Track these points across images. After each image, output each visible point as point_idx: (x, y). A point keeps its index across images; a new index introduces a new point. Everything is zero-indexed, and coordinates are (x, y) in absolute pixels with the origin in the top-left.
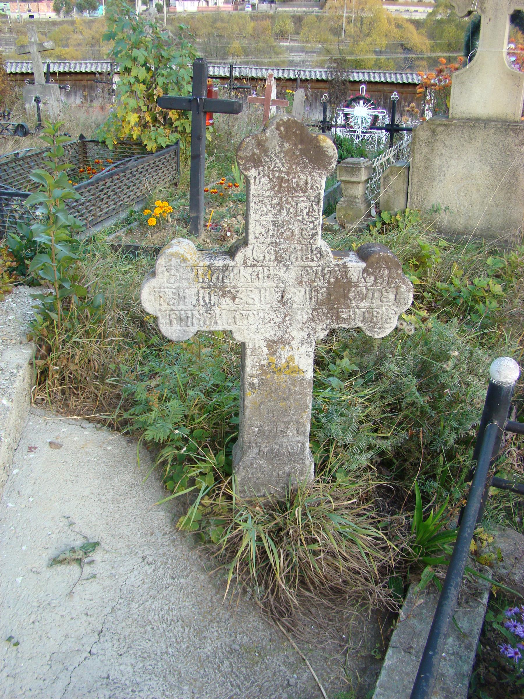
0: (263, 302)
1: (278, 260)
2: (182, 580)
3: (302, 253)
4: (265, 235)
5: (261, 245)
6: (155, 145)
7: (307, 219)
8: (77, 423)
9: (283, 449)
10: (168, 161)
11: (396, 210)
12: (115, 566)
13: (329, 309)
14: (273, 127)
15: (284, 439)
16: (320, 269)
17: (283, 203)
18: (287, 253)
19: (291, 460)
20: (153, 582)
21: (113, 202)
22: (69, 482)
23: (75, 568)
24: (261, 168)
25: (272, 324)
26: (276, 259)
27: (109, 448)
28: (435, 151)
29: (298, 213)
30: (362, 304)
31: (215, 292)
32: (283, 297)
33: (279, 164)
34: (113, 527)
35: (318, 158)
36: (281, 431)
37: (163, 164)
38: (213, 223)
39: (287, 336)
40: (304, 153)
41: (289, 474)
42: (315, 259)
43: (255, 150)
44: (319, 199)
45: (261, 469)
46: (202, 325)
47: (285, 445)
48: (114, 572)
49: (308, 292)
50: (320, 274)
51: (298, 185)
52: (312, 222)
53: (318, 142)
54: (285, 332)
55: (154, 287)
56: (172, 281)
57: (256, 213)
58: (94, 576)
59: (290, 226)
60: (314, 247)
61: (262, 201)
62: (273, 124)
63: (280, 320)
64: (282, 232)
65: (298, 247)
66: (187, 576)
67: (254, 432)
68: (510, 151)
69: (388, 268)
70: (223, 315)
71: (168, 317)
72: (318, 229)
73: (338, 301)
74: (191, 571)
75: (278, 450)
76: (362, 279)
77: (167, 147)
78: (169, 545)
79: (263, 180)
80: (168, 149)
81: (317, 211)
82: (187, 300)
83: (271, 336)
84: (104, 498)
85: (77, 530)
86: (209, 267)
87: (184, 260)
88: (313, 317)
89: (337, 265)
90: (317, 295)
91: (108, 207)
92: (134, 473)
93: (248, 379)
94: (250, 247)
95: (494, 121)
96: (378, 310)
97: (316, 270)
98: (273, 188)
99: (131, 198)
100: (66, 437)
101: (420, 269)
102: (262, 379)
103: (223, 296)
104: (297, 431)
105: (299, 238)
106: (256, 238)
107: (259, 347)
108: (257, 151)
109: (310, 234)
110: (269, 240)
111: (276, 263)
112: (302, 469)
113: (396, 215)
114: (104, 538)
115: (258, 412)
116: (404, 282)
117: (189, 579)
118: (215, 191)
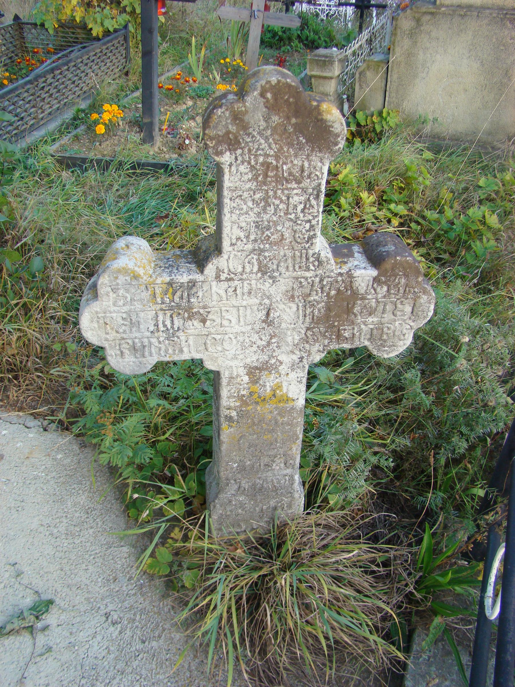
0: (242, 323)
1: (262, 271)
2: (154, 644)
3: (294, 260)
4: (245, 240)
5: (239, 254)
6: (101, 29)
7: (302, 218)
8: (20, 421)
9: (267, 483)
10: (117, 49)
11: (372, 109)
12: (74, 630)
13: (328, 327)
14: (255, 93)
15: (269, 474)
16: (318, 279)
17: (269, 197)
18: (274, 261)
19: (277, 494)
20: (120, 650)
21: (56, 101)
22: (13, 511)
23: (26, 638)
24: (239, 152)
25: (255, 348)
26: (259, 270)
27: (59, 456)
28: (418, 44)
29: (290, 210)
30: (370, 319)
31: (179, 314)
32: (268, 314)
33: (264, 145)
34: (69, 573)
35: (318, 135)
36: (265, 465)
37: (111, 52)
38: (169, 126)
39: (273, 361)
40: (299, 129)
41: (275, 509)
42: (312, 268)
43: (230, 127)
44: (319, 191)
45: (242, 505)
46: (163, 354)
47: (269, 479)
48: (72, 640)
49: (301, 308)
50: (317, 286)
51: (290, 174)
52: (309, 221)
53: (320, 114)
54: (271, 357)
55: (97, 313)
56: (121, 303)
57: (232, 212)
58: (49, 649)
59: (279, 228)
60: (311, 252)
61: (241, 196)
62: (255, 89)
63: (264, 343)
64: (267, 236)
65: (289, 254)
66: (160, 637)
67: (232, 468)
68: (504, 45)
69: (406, 276)
70: (191, 342)
71: (118, 348)
72: (317, 230)
73: (339, 316)
74: (164, 630)
75: (262, 485)
76: (372, 290)
77: (116, 31)
78: (135, 593)
79: (243, 168)
80: (116, 34)
81: (316, 207)
82: (142, 326)
83: (253, 362)
84: (56, 531)
85: (25, 581)
86: (170, 284)
87: (136, 277)
88: (307, 337)
89: (341, 274)
90: (312, 312)
91: (51, 107)
92: (90, 492)
93: (224, 412)
94: (225, 256)
95: (488, 8)
96: (389, 325)
97: (313, 281)
98: (255, 178)
99: (77, 94)
100: (8, 443)
101: (405, 192)
102: (241, 410)
103: (190, 318)
104: (285, 464)
105: (291, 242)
106: (232, 245)
107: (238, 376)
108: (233, 128)
109: (306, 236)
110: (250, 246)
111: (259, 275)
112: (291, 502)
113: (372, 116)
114: (59, 590)
115: (236, 448)
116: (425, 292)
117: (161, 641)
118: (171, 87)
